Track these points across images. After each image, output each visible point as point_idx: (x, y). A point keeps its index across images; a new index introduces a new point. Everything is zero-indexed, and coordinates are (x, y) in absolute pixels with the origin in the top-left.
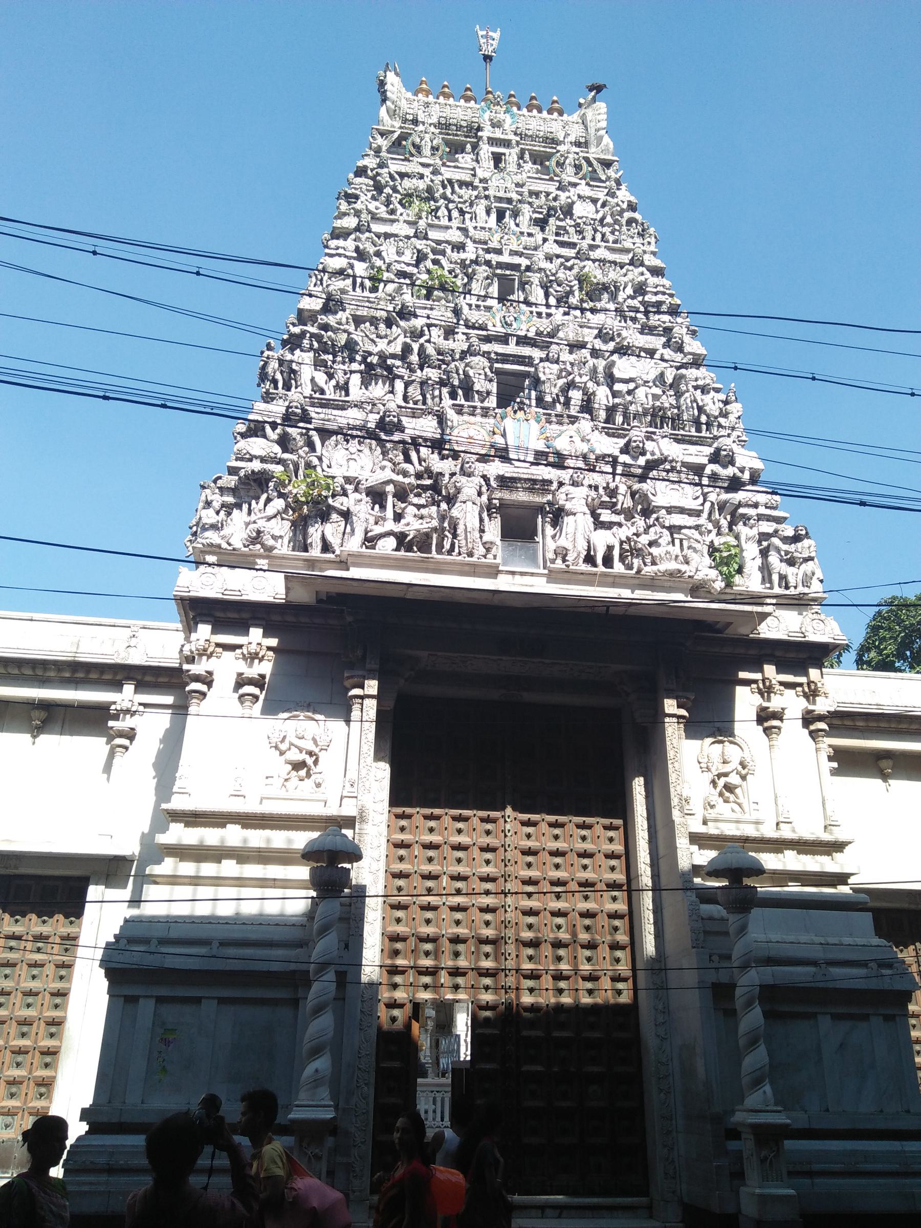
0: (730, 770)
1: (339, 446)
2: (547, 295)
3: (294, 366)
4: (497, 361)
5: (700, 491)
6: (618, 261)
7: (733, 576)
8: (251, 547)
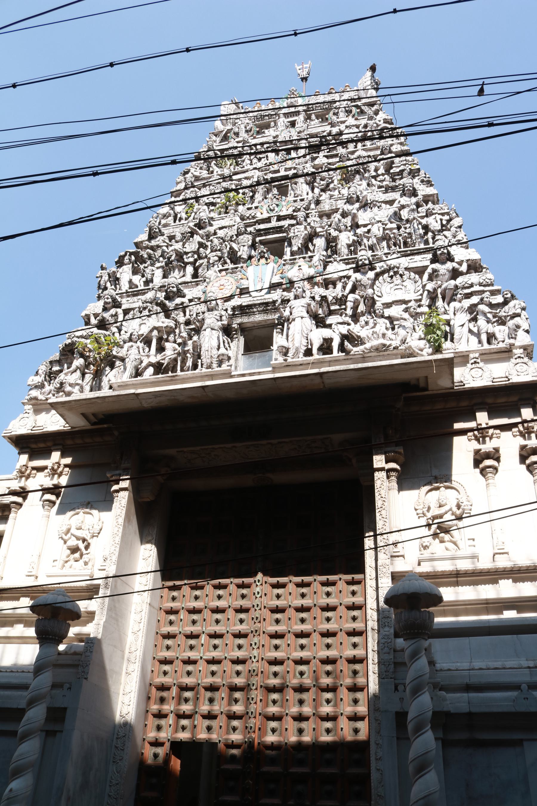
3: (118, 276)
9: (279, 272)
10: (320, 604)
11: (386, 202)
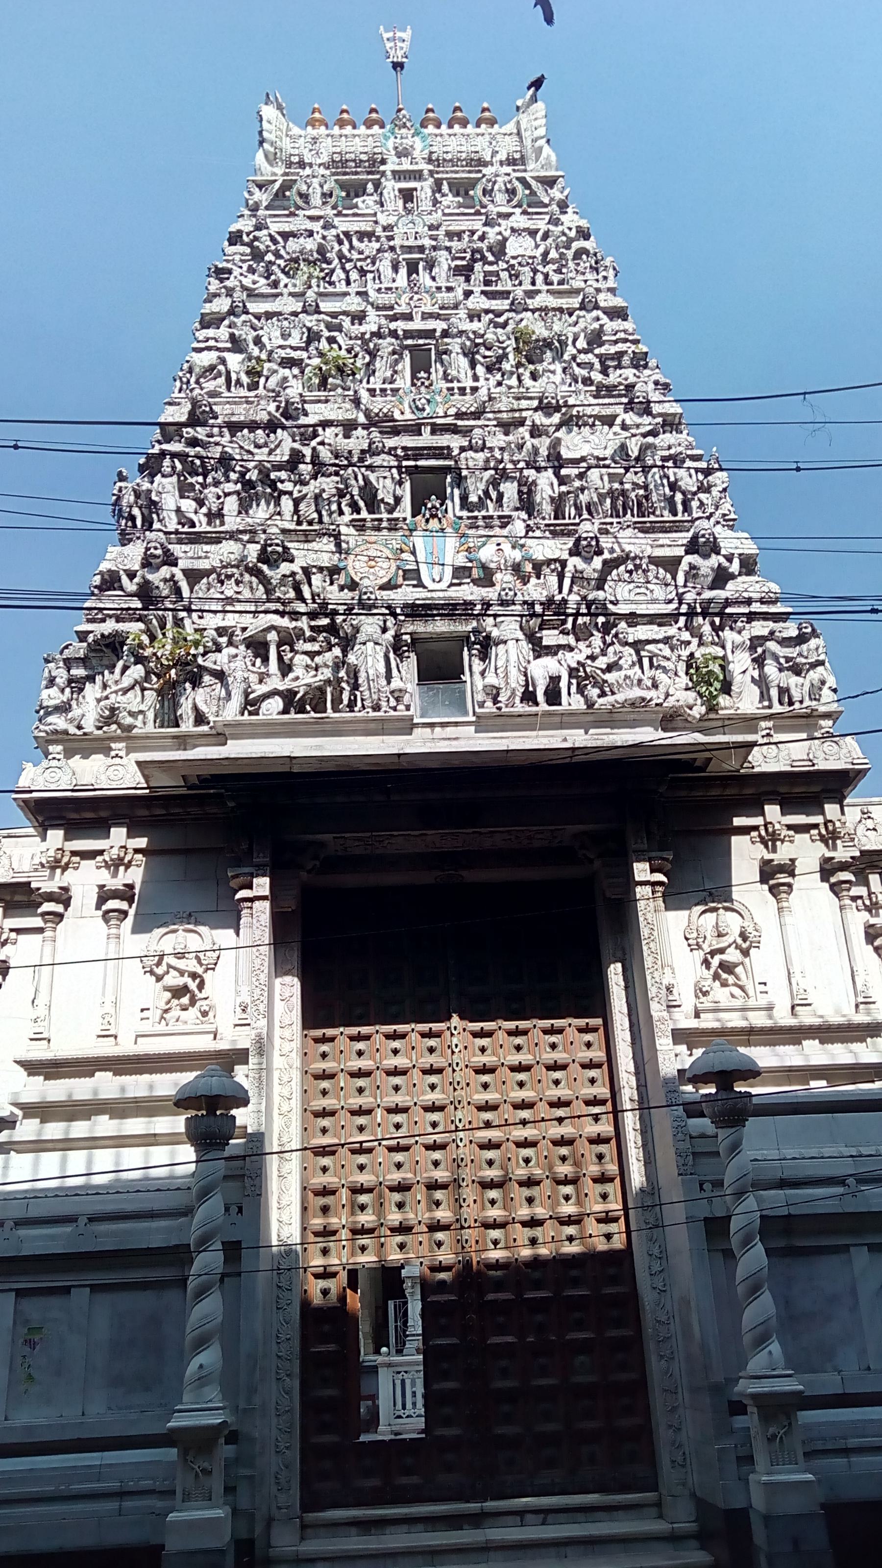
0: (726, 944)
2: (473, 364)
3: (154, 497)
4: (407, 458)
5: (674, 593)
6: (564, 306)
7: (716, 697)
8: (105, 729)
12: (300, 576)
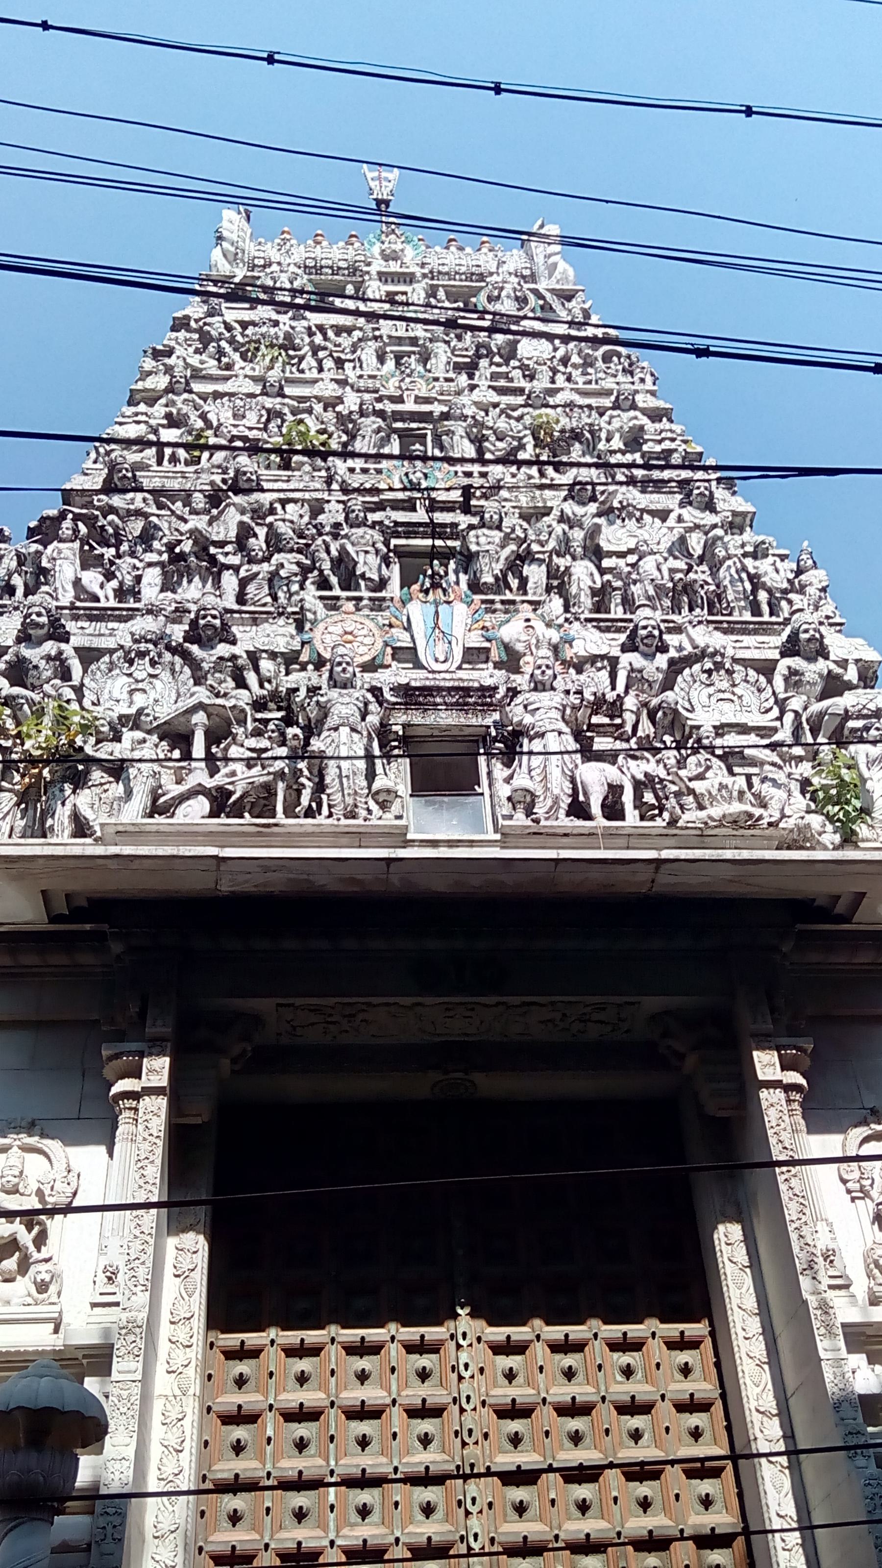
1: (116, 672)
3: (45, 563)
5: (772, 700)
6: (594, 405)
9: (476, 626)
10: (615, 1398)
11: (653, 513)
12: (243, 661)
